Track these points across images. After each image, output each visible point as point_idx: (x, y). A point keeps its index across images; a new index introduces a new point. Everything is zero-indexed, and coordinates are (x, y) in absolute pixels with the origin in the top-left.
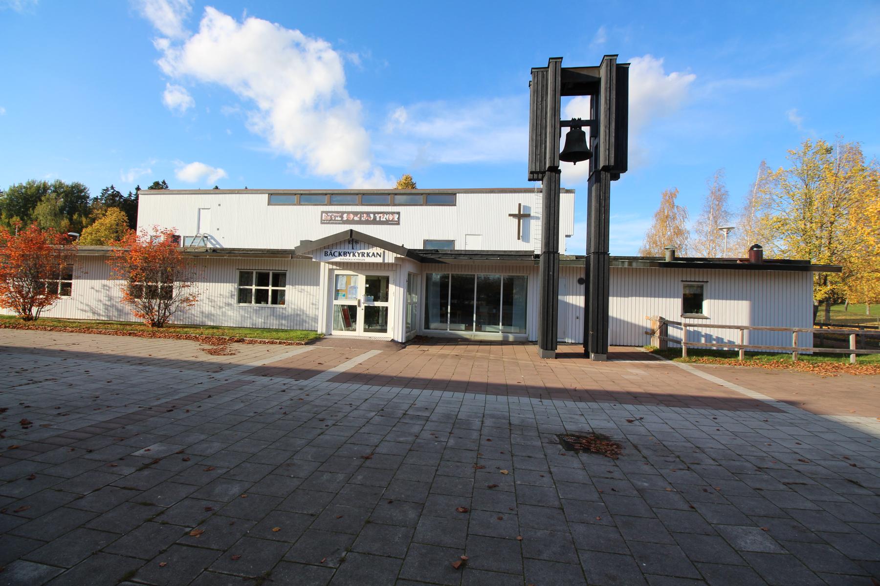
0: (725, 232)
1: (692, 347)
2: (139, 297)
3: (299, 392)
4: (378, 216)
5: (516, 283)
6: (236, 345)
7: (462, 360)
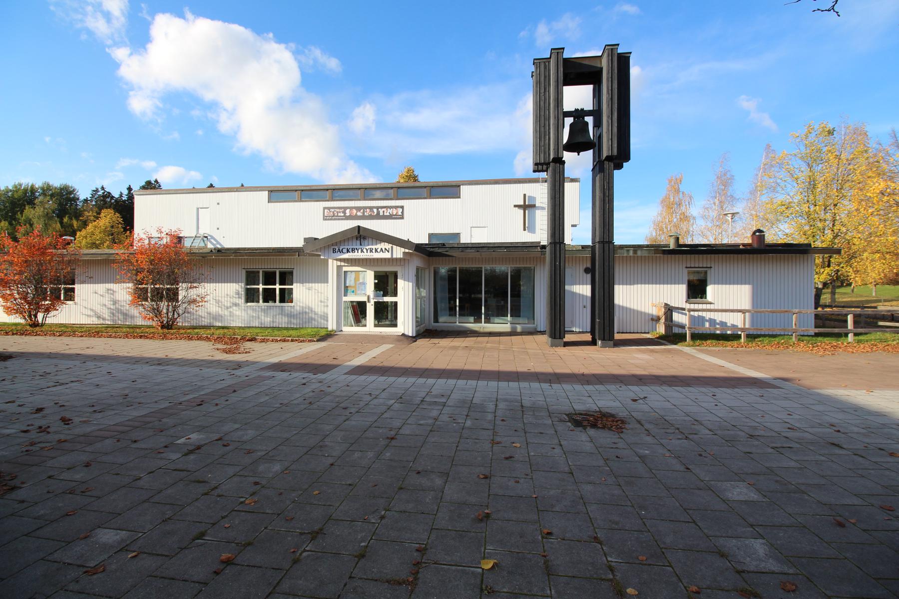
0: (729, 218)
2: (146, 300)
4: (381, 211)
6: (248, 345)
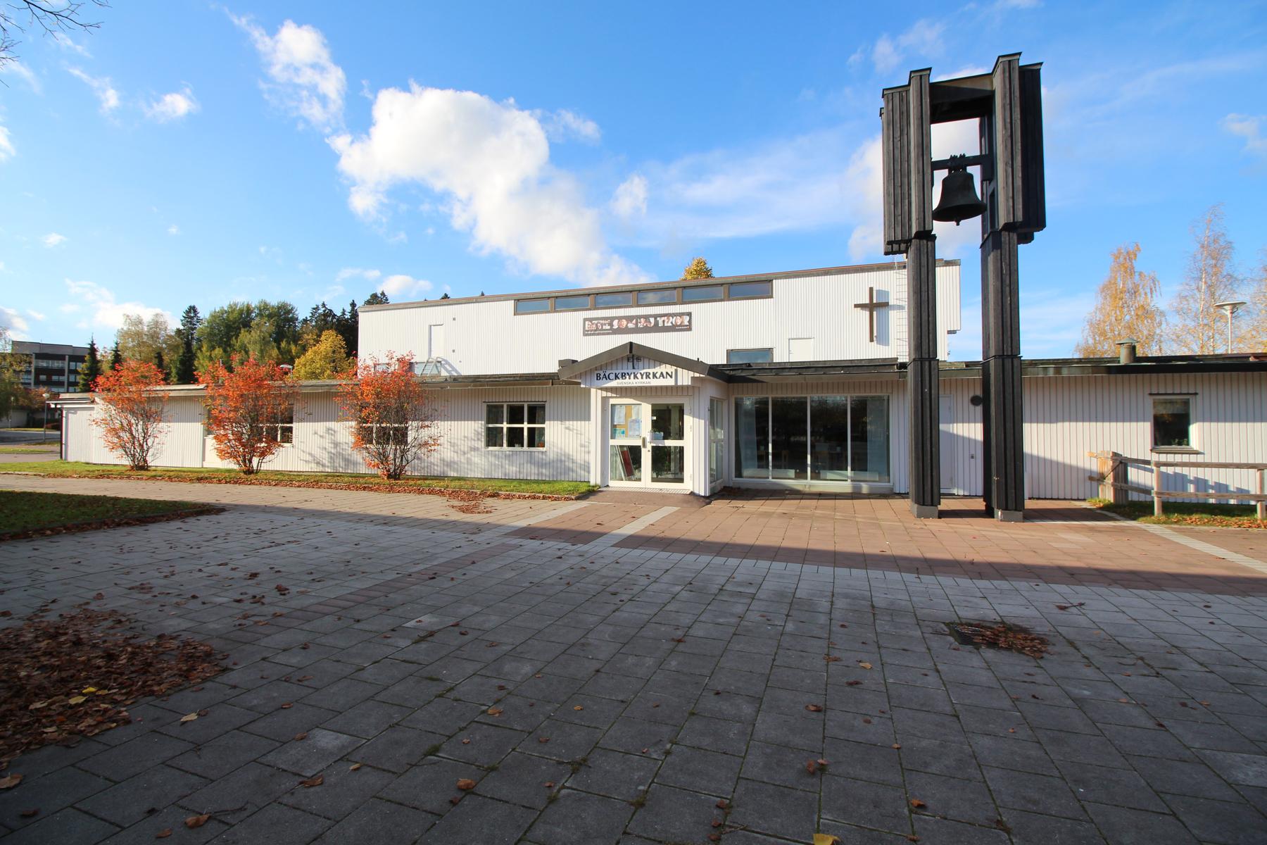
0: (1227, 312)
1: (1172, 500)
3: (579, 559)
4: (660, 320)
5: (870, 407)
6: (490, 502)
7: (794, 520)
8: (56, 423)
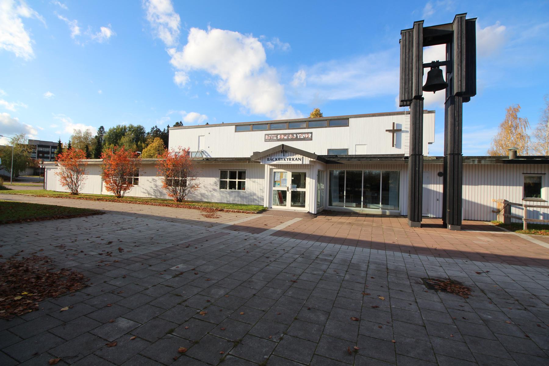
1: (531, 223)
2: (171, 185)
4: (298, 135)
6: (219, 213)
7: (354, 226)
8: (41, 172)
